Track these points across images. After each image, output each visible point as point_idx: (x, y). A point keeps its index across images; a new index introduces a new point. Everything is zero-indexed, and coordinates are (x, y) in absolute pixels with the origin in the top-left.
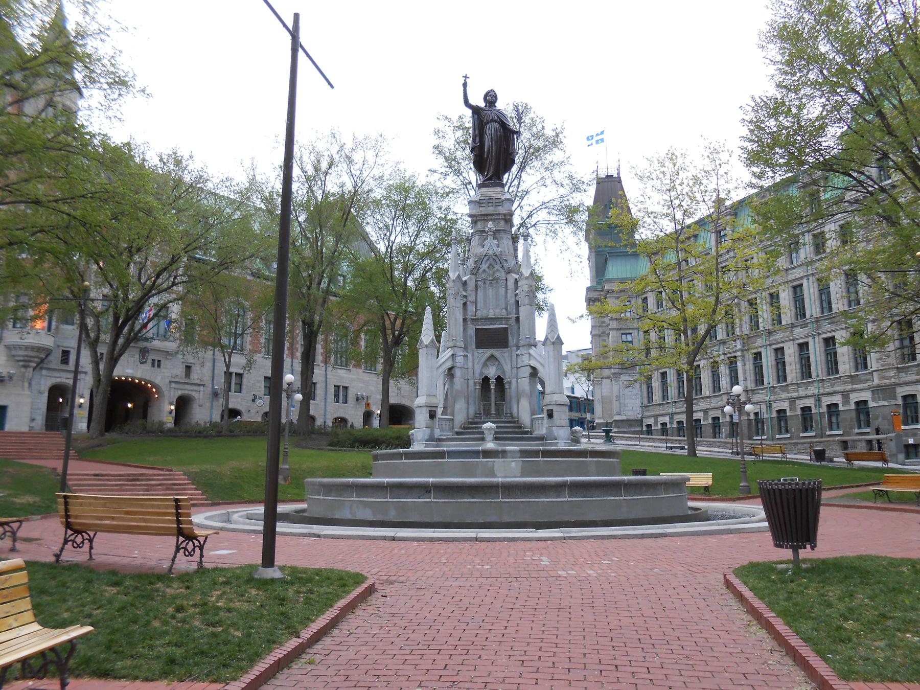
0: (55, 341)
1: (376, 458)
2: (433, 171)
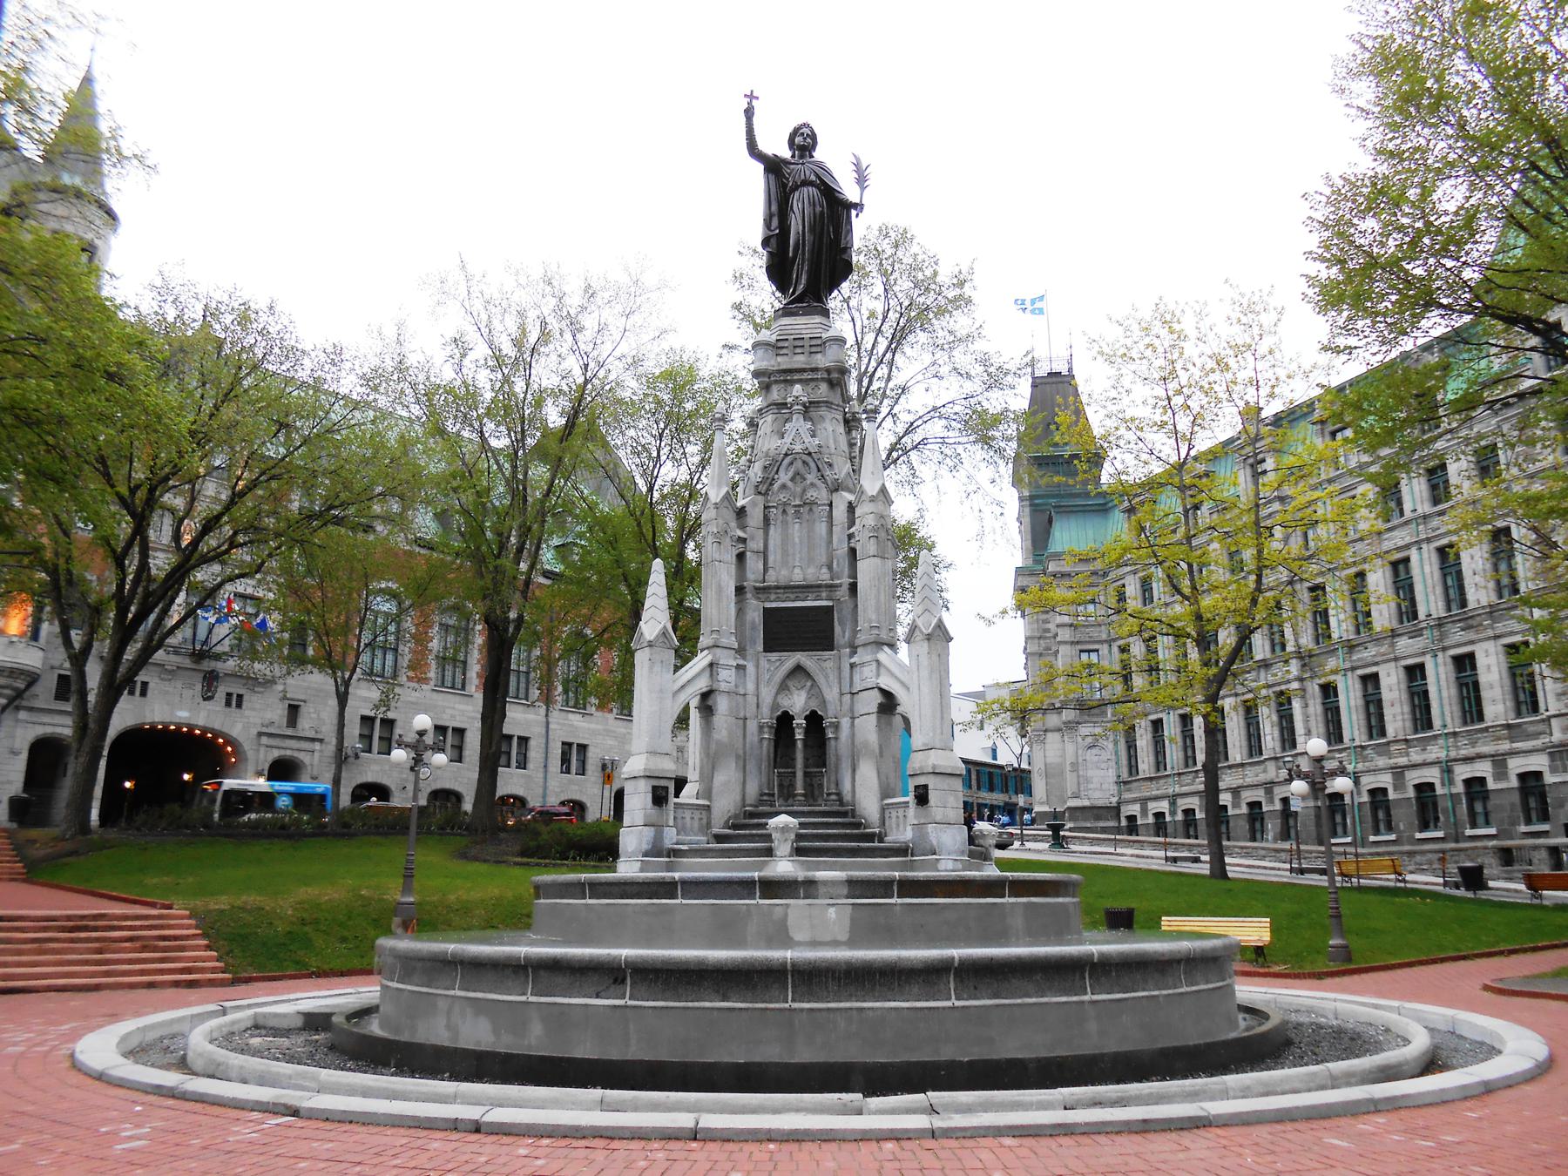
0: (45, 658)
1: (540, 890)
2: (730, 347)
